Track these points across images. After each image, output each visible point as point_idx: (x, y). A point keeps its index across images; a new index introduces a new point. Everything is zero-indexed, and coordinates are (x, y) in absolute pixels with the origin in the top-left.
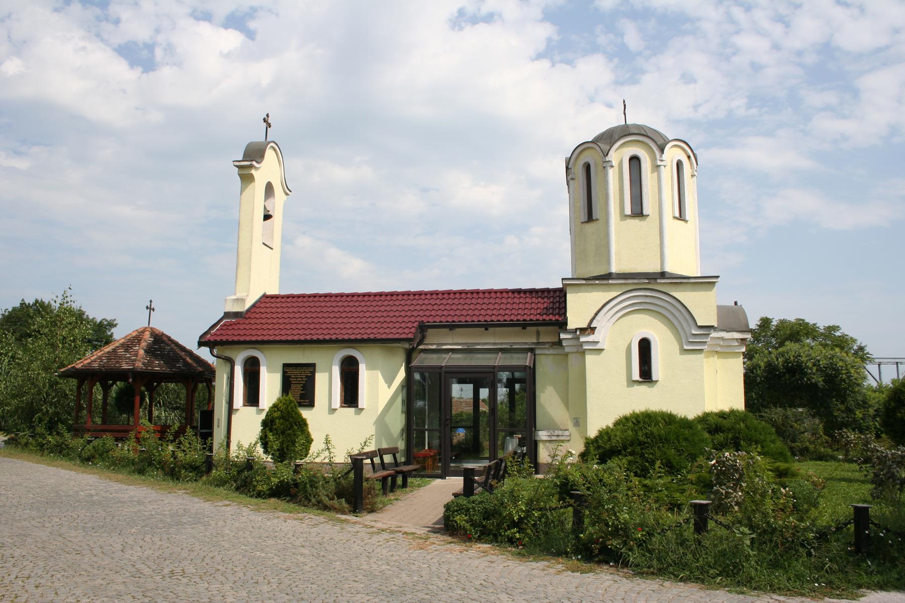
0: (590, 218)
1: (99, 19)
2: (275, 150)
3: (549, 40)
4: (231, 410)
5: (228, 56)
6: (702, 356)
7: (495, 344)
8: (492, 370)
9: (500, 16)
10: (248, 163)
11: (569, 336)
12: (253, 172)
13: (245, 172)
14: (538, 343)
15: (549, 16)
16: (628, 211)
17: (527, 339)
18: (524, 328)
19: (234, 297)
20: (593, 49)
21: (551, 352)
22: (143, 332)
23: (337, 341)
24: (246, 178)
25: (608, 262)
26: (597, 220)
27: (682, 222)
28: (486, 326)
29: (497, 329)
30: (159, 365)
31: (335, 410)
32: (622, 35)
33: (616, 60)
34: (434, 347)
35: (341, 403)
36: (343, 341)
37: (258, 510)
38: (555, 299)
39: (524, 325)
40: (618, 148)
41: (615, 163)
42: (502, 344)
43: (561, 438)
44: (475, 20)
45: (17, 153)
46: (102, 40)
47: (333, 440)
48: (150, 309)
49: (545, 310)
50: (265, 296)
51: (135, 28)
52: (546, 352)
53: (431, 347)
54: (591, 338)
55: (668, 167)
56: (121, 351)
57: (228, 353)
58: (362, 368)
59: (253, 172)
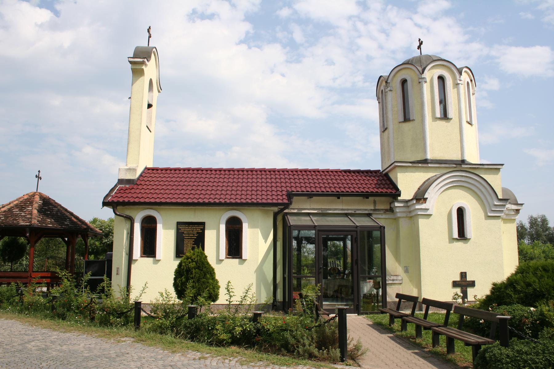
0: (406, 119)
3: (247, 33)
4: (130, 260)
5: (41, 26)
6: (500, 220)
8: (355, 229)
9: (218, 15)
10: (141, 60)
11: (402, 205)
12: (144, 67)
13: (137, 67)
14: (375, 210)
15: (249, 18)
16: (438, 115)
17: (367, 206)
18: (339, 198)
20: (274, 40)
21: (384, 216)
22: (34, 195)
23: (220, 204)
25: (425, 151)
26: (413, 120)
28: (338, 196)
32: (292, 33)
33: (288, 48)
34: (295, 211)
36: (231, 204)
39: (366, 195)
40: (430, 70)
41: (428, 80)
42: (348, 209)
43: (395, 282)
44: (203, 17)
47: (233, 285)
48: (38, 177)
49: (380, 186)
52: (380, 216)
53: (293, 211)
54: (423, 206)
56: (16, 211)
57: (128, 212)
58: (245, 226)
59: (144, 67)
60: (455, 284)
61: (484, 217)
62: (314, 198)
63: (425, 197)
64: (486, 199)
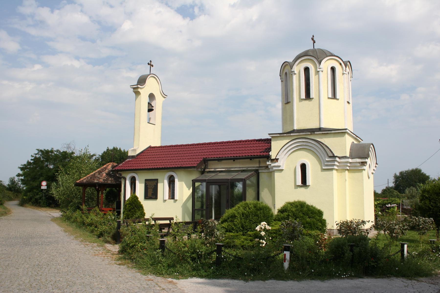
0: (308, 95)
2: (155, 77)
12: (139, 90)
13: (136, 90)
14: (259, 167)
18: (251, 160)
19: (132, 149)
24: (137, 94)
27: (335, 100)
29: (241, 160)
30: (111, 181)
31: (166, 200)
34: (213, 170)
35: (169, 197)
38: (266, 143)
39: (251, 158)
40: (298, 64)
42: (243, 167)
45: (131, 70)
46: (169, 7)
48: (150, 65)
50: (150, 147)
52: (264, 171)
55: (325, 71)
58: (176, 180)
59: (139, 90)
61: (320, 170)
62: (223, 161)
64: (322, 157)
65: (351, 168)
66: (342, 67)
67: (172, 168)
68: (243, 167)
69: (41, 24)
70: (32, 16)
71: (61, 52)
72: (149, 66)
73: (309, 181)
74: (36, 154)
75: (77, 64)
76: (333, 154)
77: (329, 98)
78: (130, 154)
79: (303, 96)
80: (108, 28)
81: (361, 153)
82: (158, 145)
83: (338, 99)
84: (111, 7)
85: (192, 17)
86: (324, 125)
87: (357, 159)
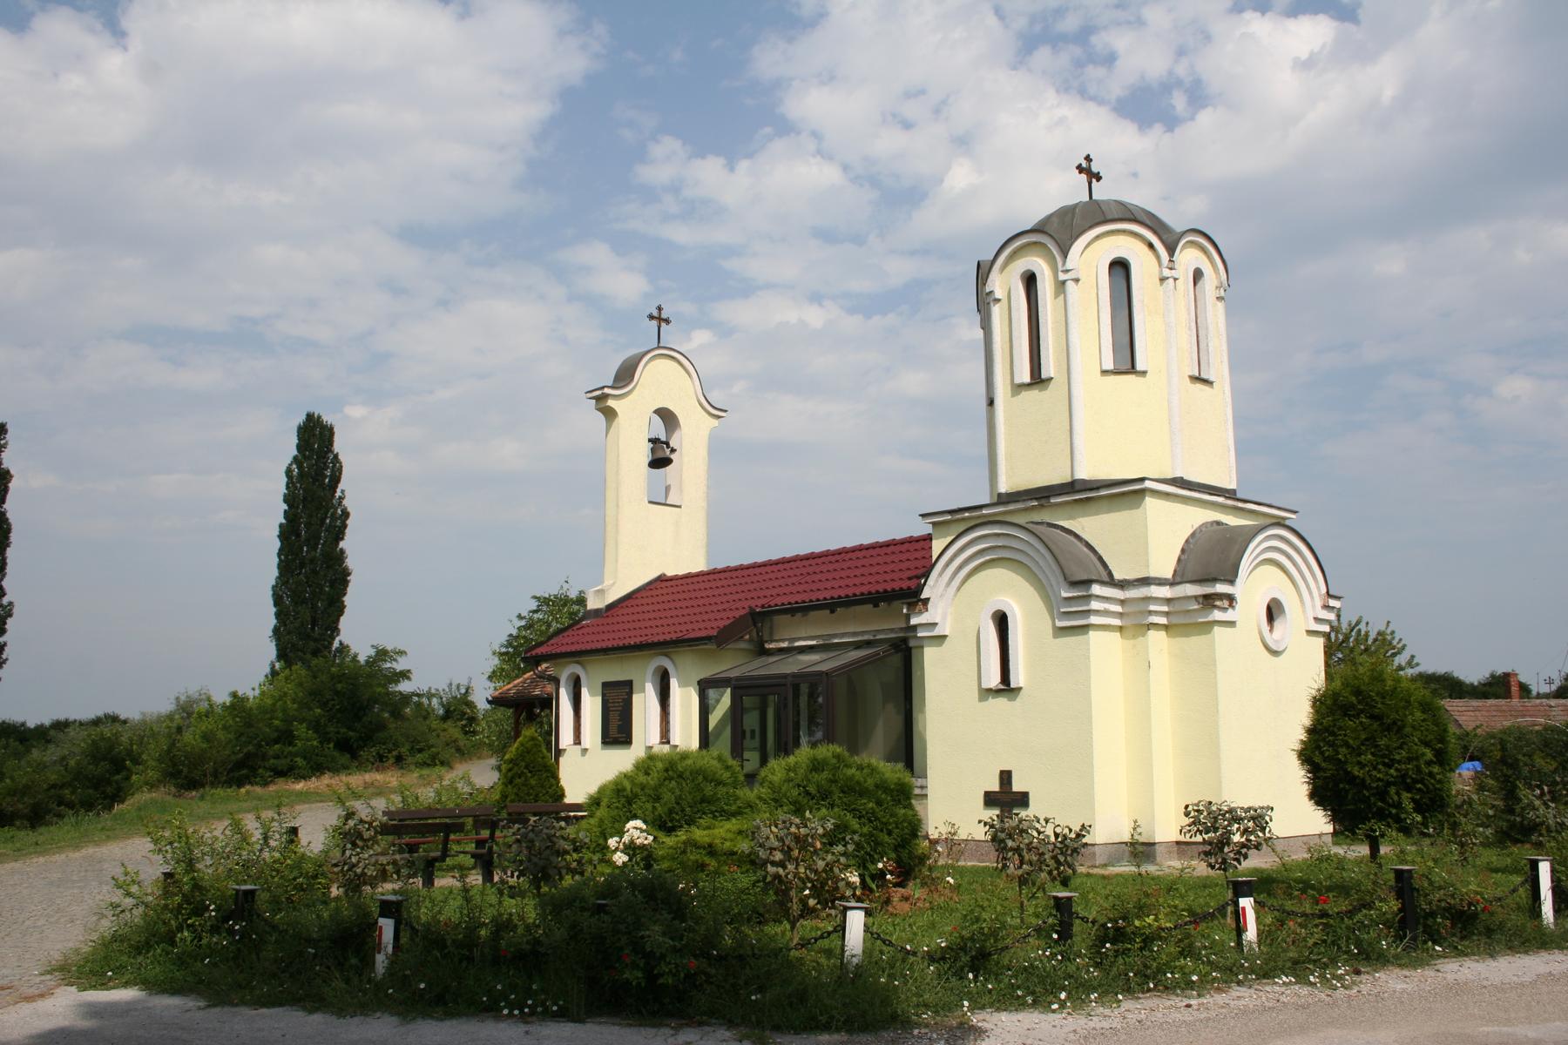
1: (1079, 64)
5: (1306, 65)
7: (855, 634)
18: (876, 606)
34: (785, 645)
37: (39, 848)
42: (863, 633)
46: (1092, 99)
50: (662, 579)
51: (1141, 56)
59: (611, 403)
60: (990, 799)
62: (812, 613)
63: (923, 596)
65: (1175, 620)
66: (1158, 257)
67: (605, 651)
68: (863, 633)
69: (698, 210)
70: (675, 188)
71: (769, 286)
72: (655, 323)
73: (1018, 677)
74: (535, 612)
75: (815, 317)
76: (1110, 574)
77: (1105, 372)
78: (593, 603)
79: (1025, 376)
80: (899, 195)
81: (1211, 565)
82: (698, 564)
83: (1144, 373)
84: (907, 125)
85: (1171, 122)
86: (1086, 471)
87: (1188, 586)
